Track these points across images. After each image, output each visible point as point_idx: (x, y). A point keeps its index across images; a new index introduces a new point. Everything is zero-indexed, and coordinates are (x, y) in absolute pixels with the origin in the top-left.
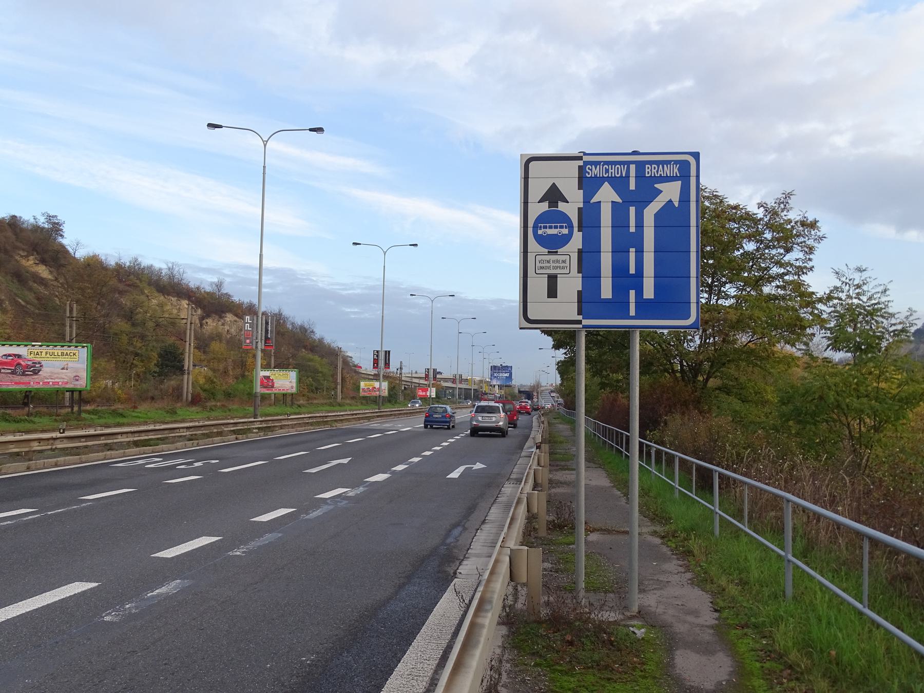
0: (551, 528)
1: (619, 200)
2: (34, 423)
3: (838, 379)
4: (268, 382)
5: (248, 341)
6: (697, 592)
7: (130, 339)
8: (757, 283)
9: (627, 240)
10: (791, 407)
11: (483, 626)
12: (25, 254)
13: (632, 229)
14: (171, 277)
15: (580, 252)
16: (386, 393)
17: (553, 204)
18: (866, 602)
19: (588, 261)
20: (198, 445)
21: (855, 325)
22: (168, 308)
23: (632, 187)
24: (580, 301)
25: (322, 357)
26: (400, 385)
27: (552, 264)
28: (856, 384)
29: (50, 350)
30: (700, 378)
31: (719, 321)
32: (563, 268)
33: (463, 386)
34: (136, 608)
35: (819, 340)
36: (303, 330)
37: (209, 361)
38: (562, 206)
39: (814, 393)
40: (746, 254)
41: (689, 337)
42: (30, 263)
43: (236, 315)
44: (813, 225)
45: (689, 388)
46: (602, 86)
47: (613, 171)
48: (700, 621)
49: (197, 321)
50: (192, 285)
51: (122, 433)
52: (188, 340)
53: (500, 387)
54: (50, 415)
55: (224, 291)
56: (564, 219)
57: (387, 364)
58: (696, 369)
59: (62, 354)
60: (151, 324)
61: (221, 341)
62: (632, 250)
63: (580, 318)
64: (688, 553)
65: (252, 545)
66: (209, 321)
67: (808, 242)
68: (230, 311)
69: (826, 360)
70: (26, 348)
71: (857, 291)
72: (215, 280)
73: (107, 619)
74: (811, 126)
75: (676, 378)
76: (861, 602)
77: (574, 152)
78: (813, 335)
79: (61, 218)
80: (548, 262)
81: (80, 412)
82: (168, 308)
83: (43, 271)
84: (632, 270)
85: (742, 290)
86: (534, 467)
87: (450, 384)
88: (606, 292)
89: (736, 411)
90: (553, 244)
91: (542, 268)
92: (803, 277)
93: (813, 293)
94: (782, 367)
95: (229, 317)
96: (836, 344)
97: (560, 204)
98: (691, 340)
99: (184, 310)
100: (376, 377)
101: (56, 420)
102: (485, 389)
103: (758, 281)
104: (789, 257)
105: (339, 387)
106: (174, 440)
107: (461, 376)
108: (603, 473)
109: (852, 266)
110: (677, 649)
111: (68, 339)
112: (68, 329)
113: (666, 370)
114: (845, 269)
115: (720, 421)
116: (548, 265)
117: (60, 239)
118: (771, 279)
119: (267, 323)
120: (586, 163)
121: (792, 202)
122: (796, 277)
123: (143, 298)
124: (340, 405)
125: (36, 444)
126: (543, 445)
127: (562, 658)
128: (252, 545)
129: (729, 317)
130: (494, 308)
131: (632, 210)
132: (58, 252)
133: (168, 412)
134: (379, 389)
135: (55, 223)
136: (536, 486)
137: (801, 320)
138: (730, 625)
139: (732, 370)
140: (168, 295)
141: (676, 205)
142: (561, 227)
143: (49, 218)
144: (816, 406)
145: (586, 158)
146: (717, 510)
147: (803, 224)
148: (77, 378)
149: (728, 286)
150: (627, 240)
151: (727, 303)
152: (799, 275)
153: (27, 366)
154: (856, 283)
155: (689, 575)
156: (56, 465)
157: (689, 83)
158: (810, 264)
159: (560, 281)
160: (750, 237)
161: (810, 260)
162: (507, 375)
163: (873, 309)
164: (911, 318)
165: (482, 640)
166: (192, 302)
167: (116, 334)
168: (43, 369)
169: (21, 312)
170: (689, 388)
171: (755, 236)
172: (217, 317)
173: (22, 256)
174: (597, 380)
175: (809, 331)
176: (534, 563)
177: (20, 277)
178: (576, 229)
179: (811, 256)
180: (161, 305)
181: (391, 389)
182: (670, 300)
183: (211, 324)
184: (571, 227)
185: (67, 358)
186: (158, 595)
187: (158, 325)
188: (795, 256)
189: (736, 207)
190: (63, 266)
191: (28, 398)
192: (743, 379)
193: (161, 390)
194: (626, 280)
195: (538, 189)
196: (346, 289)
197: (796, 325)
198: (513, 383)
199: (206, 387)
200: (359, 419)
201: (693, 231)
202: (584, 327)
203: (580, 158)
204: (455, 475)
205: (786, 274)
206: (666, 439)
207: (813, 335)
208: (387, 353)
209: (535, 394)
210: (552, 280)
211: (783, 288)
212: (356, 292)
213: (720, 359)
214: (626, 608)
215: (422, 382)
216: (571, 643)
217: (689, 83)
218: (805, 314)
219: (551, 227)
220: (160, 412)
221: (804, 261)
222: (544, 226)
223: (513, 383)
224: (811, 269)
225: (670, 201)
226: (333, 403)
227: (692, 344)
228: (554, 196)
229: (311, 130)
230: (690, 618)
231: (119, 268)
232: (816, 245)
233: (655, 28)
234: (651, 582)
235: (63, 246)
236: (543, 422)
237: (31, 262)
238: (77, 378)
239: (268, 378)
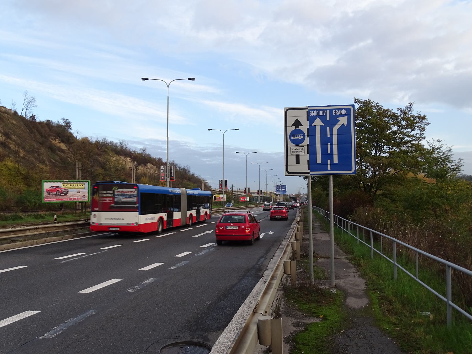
0: (301, 256)
2: (66, 217)
5: (163, 178)
6: (361, 279)
11: (273, 284)
12: (54, 138)
13: (329, 136)
14: (122, 146)
15: (308, 145)
16: (225, 200)
17: (297, 127)
18: (417, 277)
22: (121, 162)
23: (328, 119)
24: (309, 164)
25: (194, 183)
26: (232, 196)
29: (72, 184)
30: (373, 190)
33: (263, 195)
34: (139, 287)
36: (185, 170)
38: (300, 128)
42: (56, 142)
43: (153, 164)
44: (424, 118)
46: (326, 45)
47: (321, 113)
48: (359, 288)
50: (132, 150)
51: (29, 230)
53: (281, 195)
54: (73, 214)
55: (147, 153)
56: (301, 132)
57: (226, 186)
59: (77, 185)
60: (113, 170)
61: (146, 177)
62: (329, 144)
63: (309, 171)
64: (359, 265)
65: (178, 266)
66: (140, 167)
67: (422, 126)
68: (150, 162)
70: (61, 183)
72: (142, 147)
73: (129, 291)
74: (431, 61)
75: (361, 191)
76: (415, 276)
77: (305, 106)
79: (70, 120)
81: (86, 212)
82: (121, 162)
83: (63, 146)
84: (329, 152)
85: (391, 149)
86: (295, 232)
87: (256, 195)
88: (319, 160)
90: (297, 143)
92: (420, 142)
95: (150, 165)
97: (300, 127)
98: (367, 173)
99: (129, 163)
100: (221, 192)
101: (75, 216)
102: (273, 196)
104: (413, 133)
107: (261, 191)
109: (435, 139)
111: (77, 178)
112: (77, 173)
113: (357, 187)
114: (432, 140)
117: (70, 131)
119: (171, 169)
120: (310, 110)
122: (417, 142)
123: (109, 157)
125: (41, 230)
126: (300, 223)
127: (304, 299)
128: (178, 266)
130: (276, 157)
131: (328, 128)
132: (69, 137)
134: (222, 198)
135: (67, 123)
136: (297, 240)
138: (370, 290)
140: (121, 155)
141: (346, 125)
142: (301, 136)
143: (65, 120)
145: (309, 108)
146: (372, 248)
147: (419, 117)
148: (84, 196)
149: (385, 147)
150: (326, 141)
151: (385, 155)
153: (62, 191)
154: (437, 147)
155: (358, 273)
156: (45, 242)
157: (369, 41)
160: (394, 124)
161: (423, 134)
162: (284, 189)
163: (445, 159)
164: (460, 163)
165: (273, 287)
167: (97, 175)
168: (69, 192)
169: (53, 165)
172: (144, 165)
173: (53, 139)
176: (293, 267)
177: (52, 149)
178: (306, 136)
179: (424, 132)
181: (228, 198)
182: (345, 161)
183: (141, 169)
184: (304, 136)
185: (80, 187)
186: (146, 283)
187: (117, 170)
188: (416, 132)
189: (388, 110)
190: (72, 143)
191: (62, 206)
194: (327, 156)
195: (291, 121)
196: (203, 150)
198: (287, 193)
201: (353, 136)
202: (311, 174)
203: (307, 109)
205: (412, 141)
206: (356, 219)
208: (226, 181)
209: (298, 198)
210: (298, 157)
212: (209, 151)
213: (382, 181)
214: (330, 284)
216: (307, 294)
217: (369, 41)
219: (296, 136)
221: (421, 134)
222: (294, 134)
223: (287, 193)
224: (424, 138)
225: (343, 124)
227: (368, 175)
228: (297, 123)
230: (355, 288)
231: (97, 143)
232: (426, 127)
233: (351, 15)
235: (71, 134)
236: (301, 212)
237: (57, 142)
238: (84, 196)
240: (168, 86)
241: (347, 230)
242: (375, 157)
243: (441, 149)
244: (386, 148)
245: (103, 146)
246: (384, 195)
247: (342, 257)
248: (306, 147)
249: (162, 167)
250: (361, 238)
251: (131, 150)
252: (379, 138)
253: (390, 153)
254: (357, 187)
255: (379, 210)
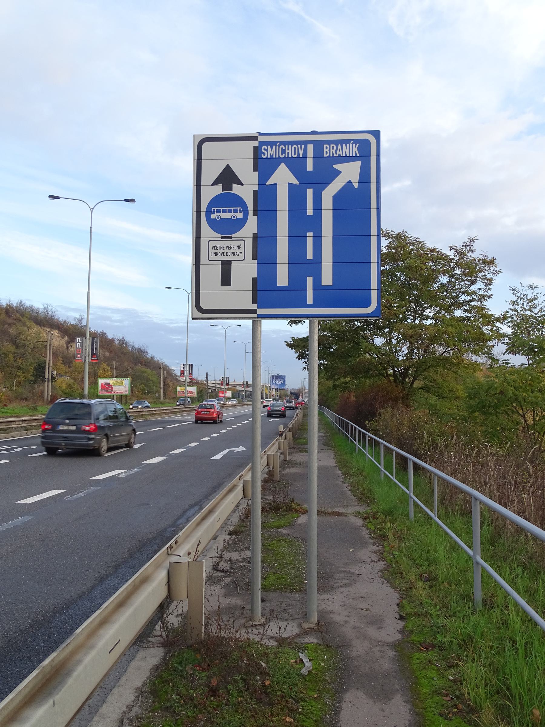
1: (296, 182)
3: (515, 376)
4: (108, 387)
5: (79, 356)
7: (15, 357)
8: (449, 309)
9: (304, 223)
10: (476, 400)
14: (46, 314)
15: (255, 237)
16: (195, 395)
17: (227, 186)
19: (263, 245)
20: (31, 434)
21: (529, 332)
23: (310, 167)
27: (226, 251)
28: (531, 380)
30: (407, 380)
31: (421, 335)
32: (237, 254)
35: (499, 349)
36: (140, 351)
37: (71, 373)
38: (236, 189)
39: (496, 388)
40: (442, 286)
41: (399, 348)
44: (492, 262)
45: (400, 388)
47: (290, 152)
49: (65, 345)
52: (48, 357)
53: (277, 390)
56: (238, 201)
57: (190, 374)
58: (405, 375)
62: (310, 234)
63: (255, 306)
64: (384, 537)
67: (488, 276)
69: (505, 362)
71: (530, 304)
75: (390, 381)
78: (493, 346)
80: (222, 248)
84: (310, 256)
87: (241, 389)
88: (283, 278)
89: (432, 405)
90: (225, 229)
91: (215, 254)
93: (492, 315)
94: (470, 371)
96: (512, 350)
98: (400, 351)
99: (57, 341)
103: (451, 306)
105: (162, 391)
106: (11, 430)
108: (331, 454)
110: (347, 690)
113: (382, 375)
115: (420, 413)
116: (222, 251)
118: (460, 305)
120: (262, 143)
121: (476, 245)
124: (161, 403)
129: (428, 331)
131: (310, 192)
133: (30, 409)
137: (483, 334)
139: (431, 374)
140: (44, 326)
141: (356, 186)
142: (236, 211)
144: (498, 400)
145: (261, 139)
147: (485, 262)
149: (428, 310)
150: (304, 223)
151: (429, 322)
152: (481, 302)
154: (529, 297)
157: (407, 183)
158: (490, 293)
159: (234, 268)
160: (444, 272)
161: (489, 289)
162: (282, 382)
166: (61, 331)
170: (400, 388)
171: (449, 273)
174: (330, 383)
175: (490, 343)
178: (251, 213)
180: (38, 333)
184: (245, 212)
188: (479, 286)
189: (433, 250)
192: (440, 380)
193: (33, 393)
195: (212, 171)
197: (480, 338)
198: (286, 387)
199: (67, 391)
200: (169, 413)
204: (217, 457)
206: (379, 428)
207: (493, 346)
208: (191, 366)
209: (301, 395)
210: (226, 267)
211: (469, 312)
215: (219, 386)
216: (214, 692)
217: (407, 183)
218: (486, 329)
219: (224, 211)
220: (24, 408)
223: (286, 387)
224: (490, 296)
225: (350, 182)
226: (156, 402)
227: (400, 354)
228: (228, 178)
229: (126, 200)
232: (494, 278)
234: (342, 575)
238: (126, 391)
239: (108, 384)
240: (92, 210)
241: (364, 448)
242: (413, 326)
243: (536, 302)
244: (429, 312)
245: (18, 312)
246: (426, 389)
247: (351, 510)
248: (250, 243)
249: (78, 339)
250: (388, 467)
251: (61, 320)
252: (418, 296)
253: (435, 318)
254: (382, 375)
255: (420, 412)
